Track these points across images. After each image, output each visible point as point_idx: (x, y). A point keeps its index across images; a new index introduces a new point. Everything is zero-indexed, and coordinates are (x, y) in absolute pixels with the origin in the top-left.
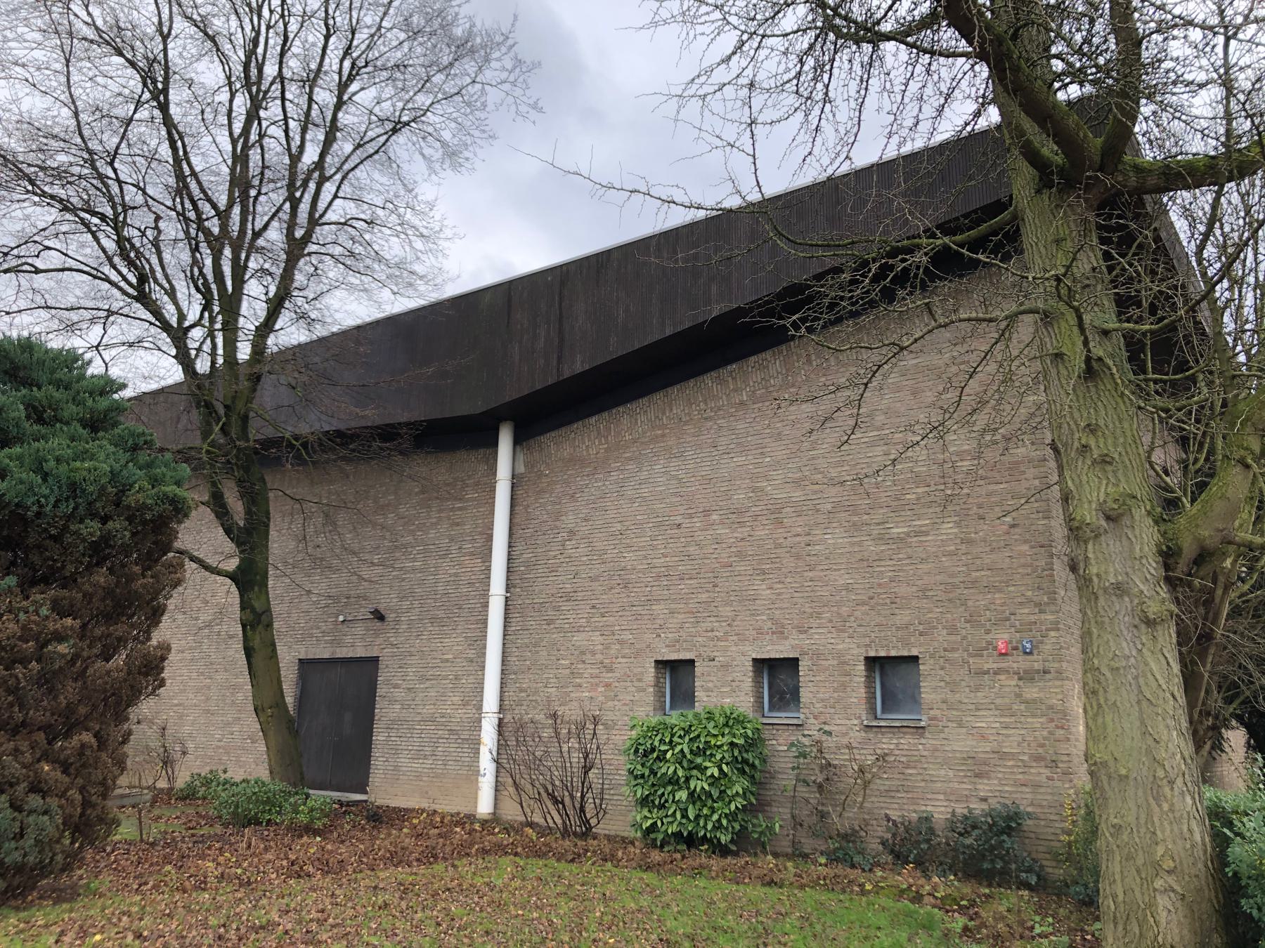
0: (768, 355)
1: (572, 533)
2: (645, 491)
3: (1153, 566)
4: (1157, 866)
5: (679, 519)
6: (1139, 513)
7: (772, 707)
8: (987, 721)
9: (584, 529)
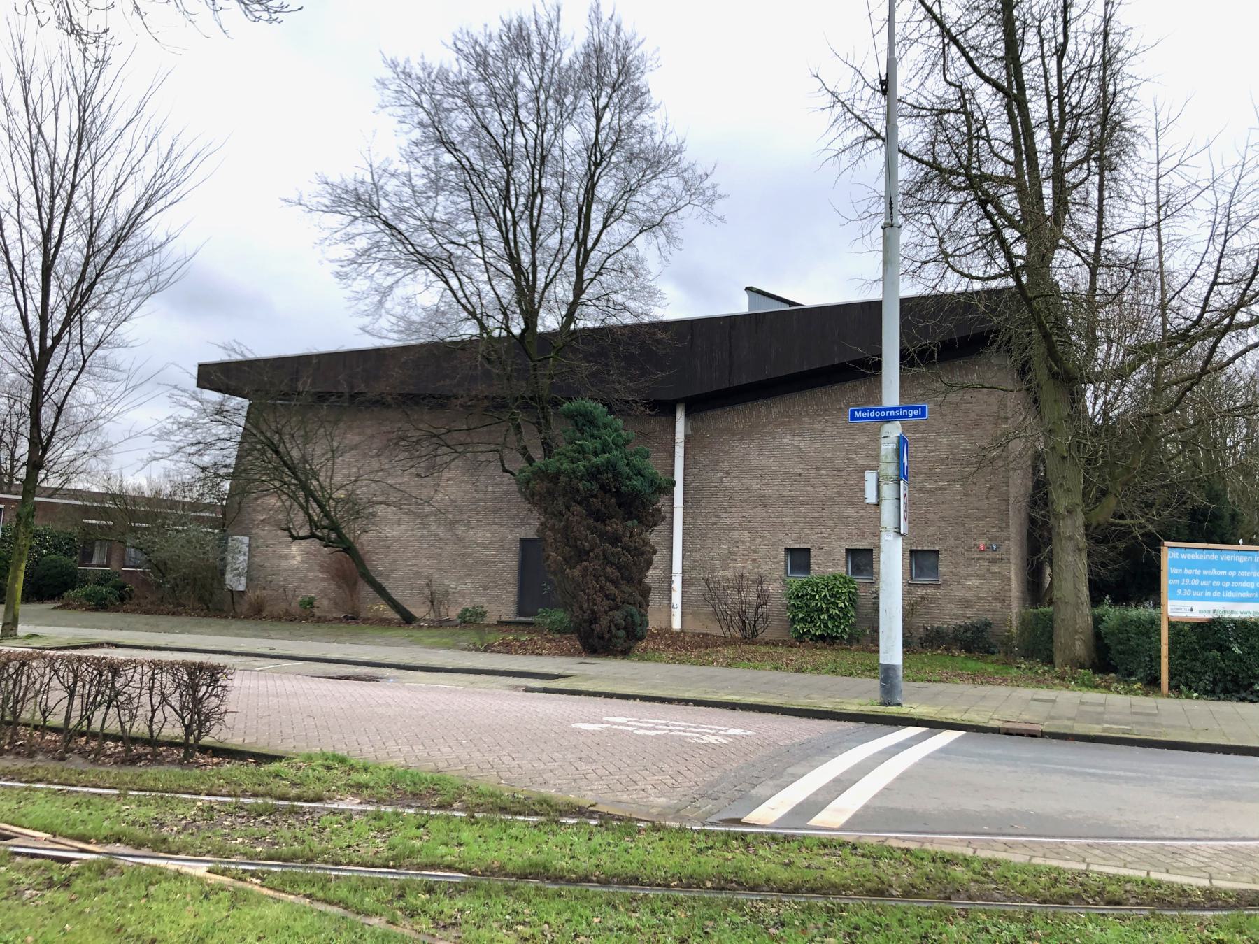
0: (857, 383)
1: (727, 474)
2: (777, 453)
3: (1082, 530)
4: (1076, 632)
5: (800, 471)
6: (1079, 510)
7: (853, 573)
8: (972, 582)
9: (736, 472)
